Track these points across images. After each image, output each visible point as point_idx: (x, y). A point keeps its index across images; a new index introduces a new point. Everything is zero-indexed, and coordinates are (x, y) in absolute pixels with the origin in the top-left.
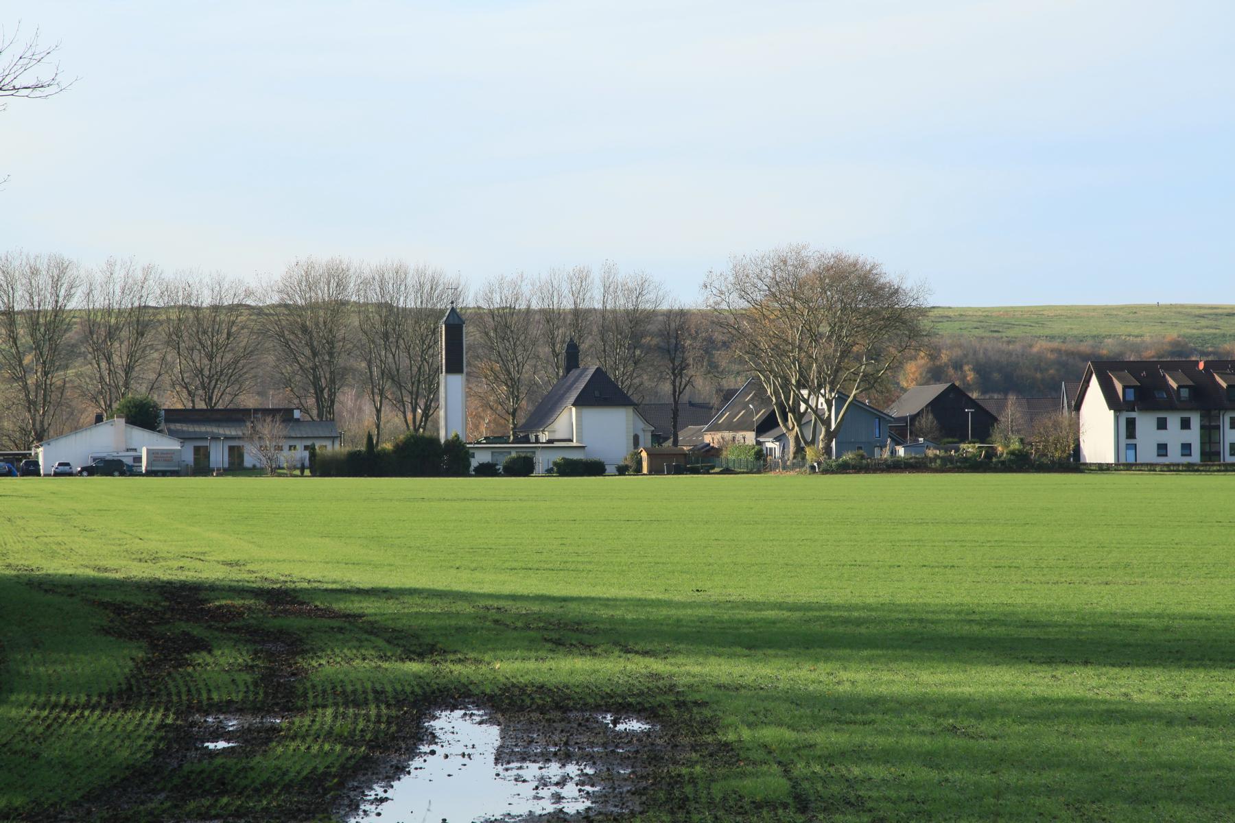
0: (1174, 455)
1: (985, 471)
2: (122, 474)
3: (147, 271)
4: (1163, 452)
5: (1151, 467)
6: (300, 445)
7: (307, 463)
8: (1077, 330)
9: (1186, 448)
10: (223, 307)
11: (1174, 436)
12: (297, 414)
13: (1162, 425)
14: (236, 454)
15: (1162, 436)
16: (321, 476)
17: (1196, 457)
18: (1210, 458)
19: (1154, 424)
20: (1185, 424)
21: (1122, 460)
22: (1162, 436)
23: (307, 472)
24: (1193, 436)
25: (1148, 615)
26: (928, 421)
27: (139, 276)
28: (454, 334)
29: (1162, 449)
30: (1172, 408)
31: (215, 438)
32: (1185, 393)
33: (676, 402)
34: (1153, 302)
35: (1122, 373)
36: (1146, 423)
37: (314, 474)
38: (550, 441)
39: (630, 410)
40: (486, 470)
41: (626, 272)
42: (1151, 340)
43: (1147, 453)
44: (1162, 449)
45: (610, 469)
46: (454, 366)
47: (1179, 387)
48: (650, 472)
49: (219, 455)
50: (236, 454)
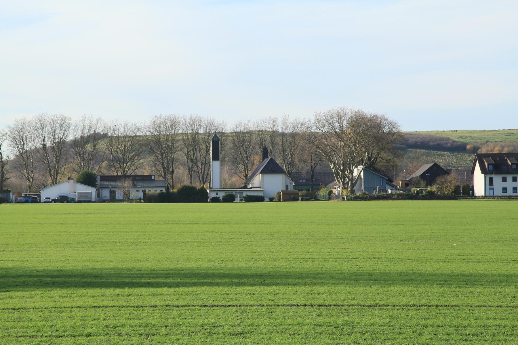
1: (415, 199)
2: (68, 202)
4: (505, 191)
6: (141, 190)
7: (142, 198)
10: (286, 134)
12: (153, 177)
13: (504, 180)
14: (113, 193)
15: (505, 184)
16: (293, 201)
19: (501, 179)
21: (488, 195)
22: (505, 184)
23: (142, 201)
25: (55, 271)
27: (94, 122)
28: (216, 143)
29: (505, 190)
30: (508, 172)
31: (119, 188)
32: (514, 166)
33: (313, 172)
34: (501, 129)
35: (489, 159)
36: (497, 179)
37: (145, 202)
38: (251, 188)
39: (284, 175)
40: (215, 200)
43: (498, 192)
44: (505, 190)
45: (267, 199)
46: (216, 157)
47: (512, 164)
48: (283, 201)
49: (106, 194)
50: (113, 193)
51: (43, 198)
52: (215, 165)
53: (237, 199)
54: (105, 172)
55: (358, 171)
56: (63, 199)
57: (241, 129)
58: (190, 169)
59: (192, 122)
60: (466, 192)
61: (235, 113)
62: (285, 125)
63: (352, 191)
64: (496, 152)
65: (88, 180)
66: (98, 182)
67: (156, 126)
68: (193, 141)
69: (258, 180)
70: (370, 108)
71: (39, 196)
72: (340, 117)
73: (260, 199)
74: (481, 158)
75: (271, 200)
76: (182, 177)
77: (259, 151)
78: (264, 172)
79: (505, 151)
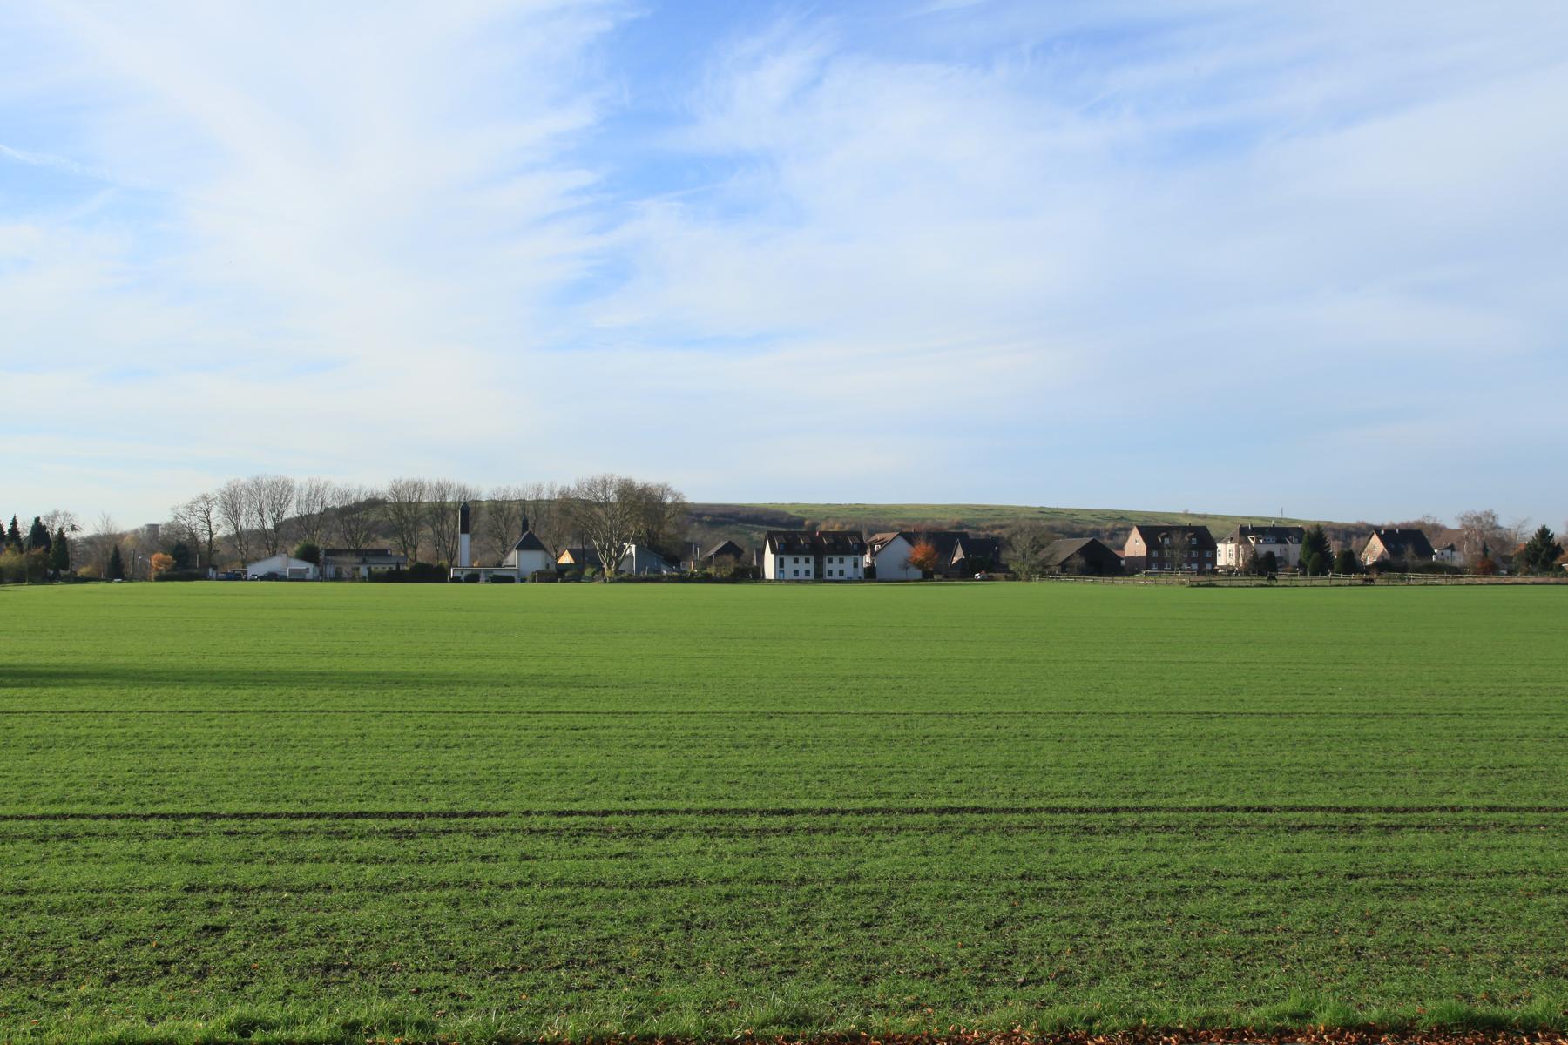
0: (802, 576)
3: (326, 484)
5: (790, 582)
8: (915, 515)
9: (807, 573)
11: (802, 566)
13: (796, 561)
15: (796, 567)
17: (812, 576)
18: (819, 577)
20: (807, 561)
22: (796, 567)
24: (811, 567)
26: (1080, 561)
28: (467, 512)
29: (796, 573)
30: (800, 553)
36: (789, 560)
40: (456, 580)
41: (1477, 507)
42: (948, 521)
43: (789, 575)
44: (796, 573)
46: (465, 530)
51: (249, 575)
52: (465, 539)
53: (482, 579)
54: (333, 544)
55: (631, 549)
56: (272, 577)
57: (499, 497)
58: (437, 544)
59: (440, 487)
60: (757, 575)
61: (489, 481)
62: (551, 492)
63: (617, 572)
64: (836, 529)
65: (309, 554)
66: (322, 557)
67: (1418, 523)
68: (440, 511)
69: (513, 558)
70: (643, 476)
71: (245, 572)
72: (605, 484)
73: (510, 580)
74: (771, 537)
75: (523, 581)
76: (424, 553)
77: (519, 522)
78: (522, 547)
79: (847, 528)
